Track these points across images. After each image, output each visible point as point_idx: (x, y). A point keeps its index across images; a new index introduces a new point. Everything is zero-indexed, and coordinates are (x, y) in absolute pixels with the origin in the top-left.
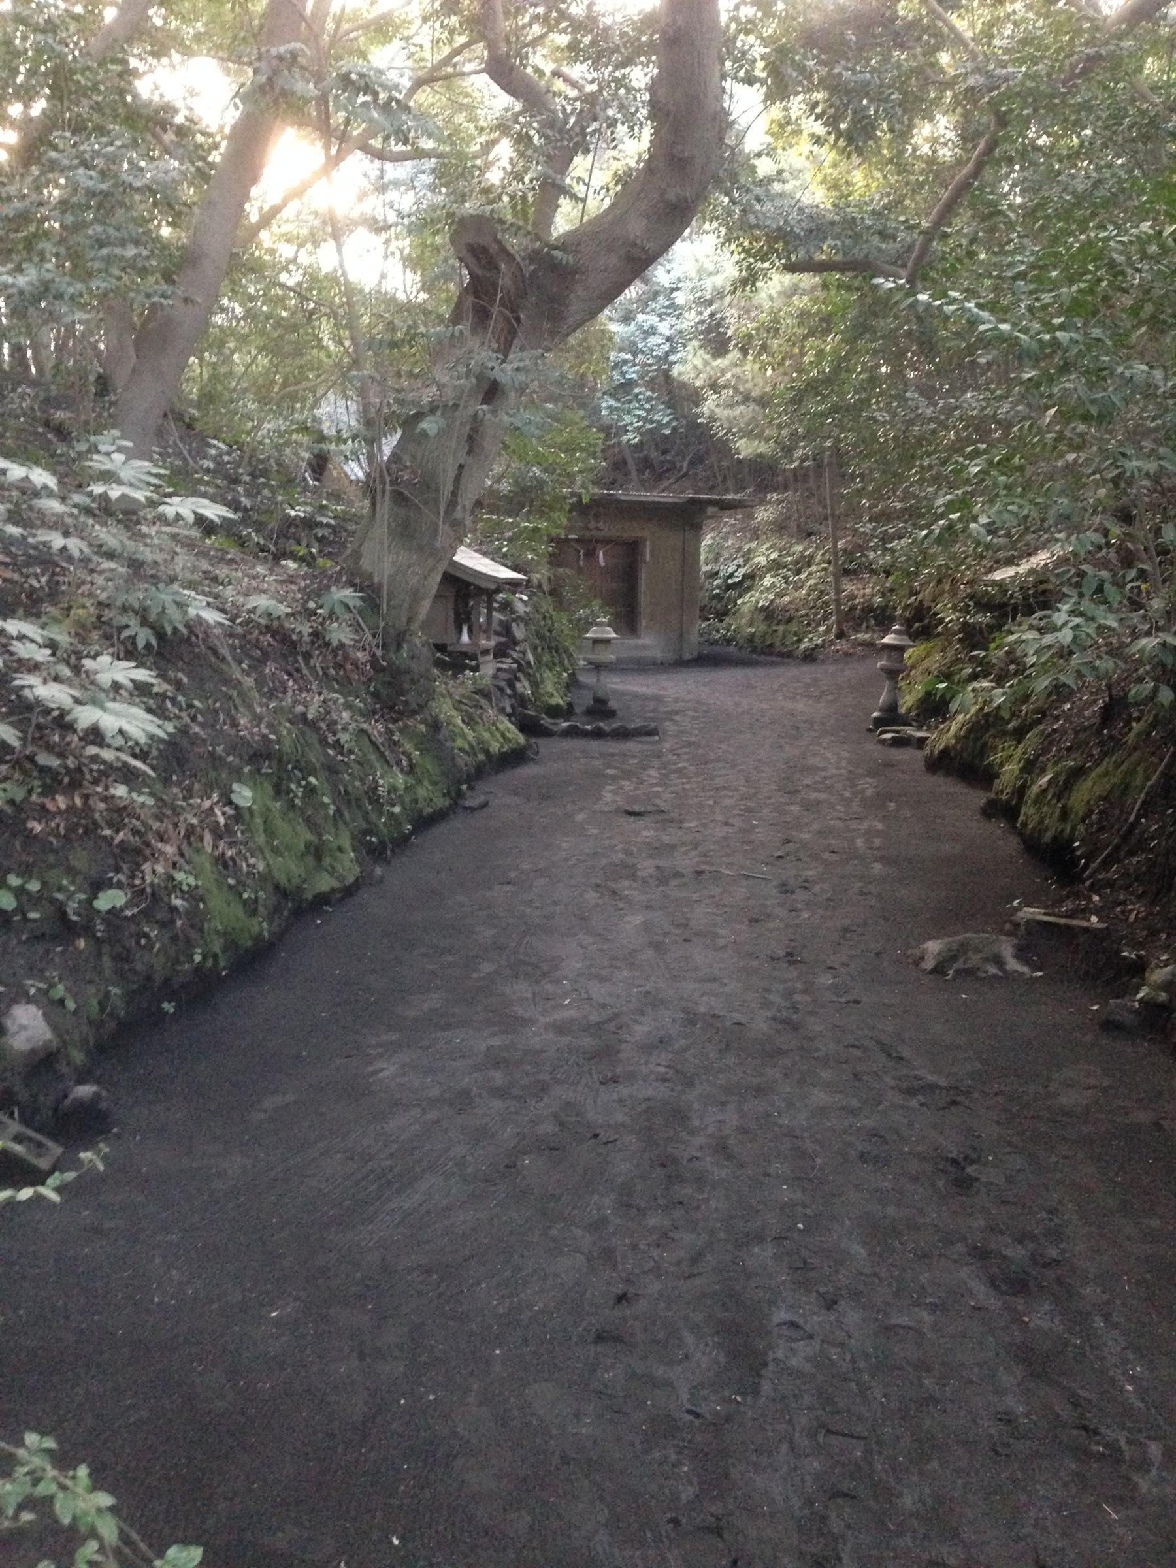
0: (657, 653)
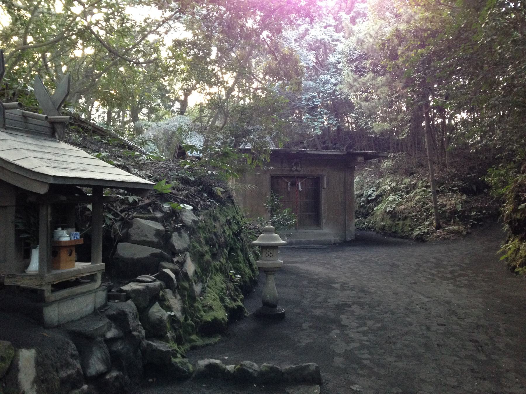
0: (332, 238)
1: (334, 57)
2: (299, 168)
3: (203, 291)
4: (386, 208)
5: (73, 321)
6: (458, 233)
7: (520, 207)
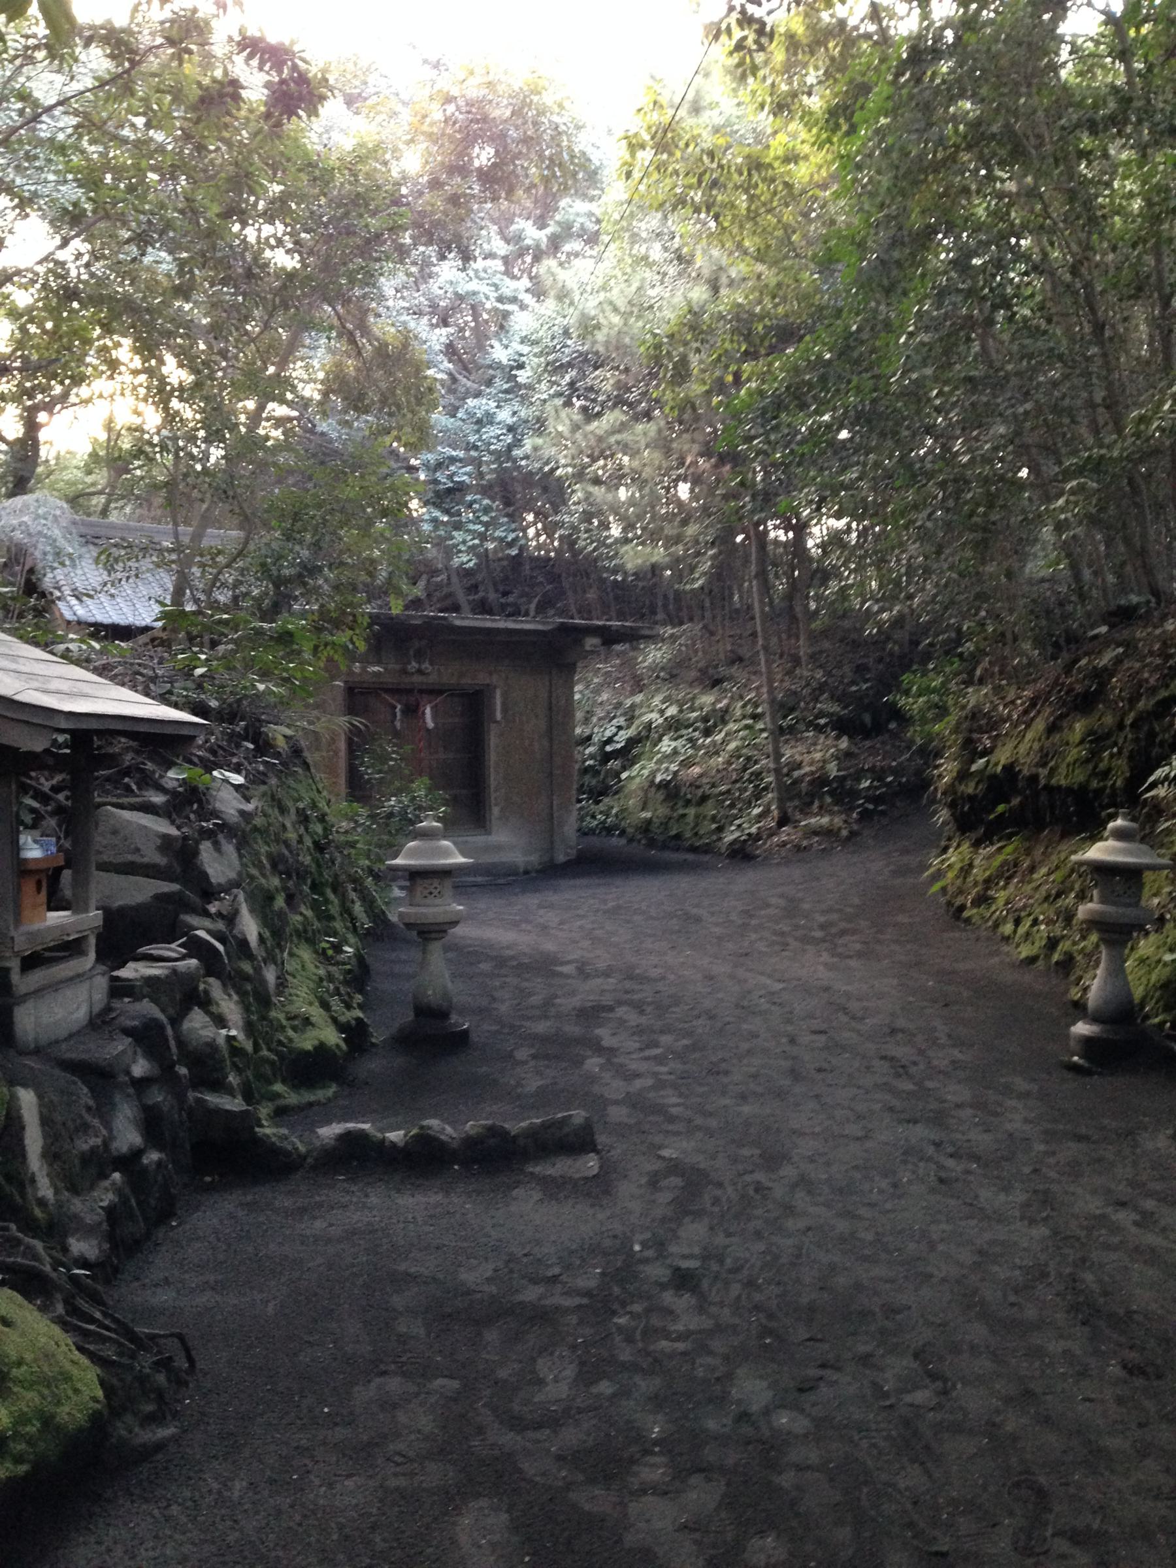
1: (506, 347)
2: (426, 666)
3: (282, 984)
4: (653, 774)
5: (57, 1042)
6: (828, 833)
7: (974, 768)
